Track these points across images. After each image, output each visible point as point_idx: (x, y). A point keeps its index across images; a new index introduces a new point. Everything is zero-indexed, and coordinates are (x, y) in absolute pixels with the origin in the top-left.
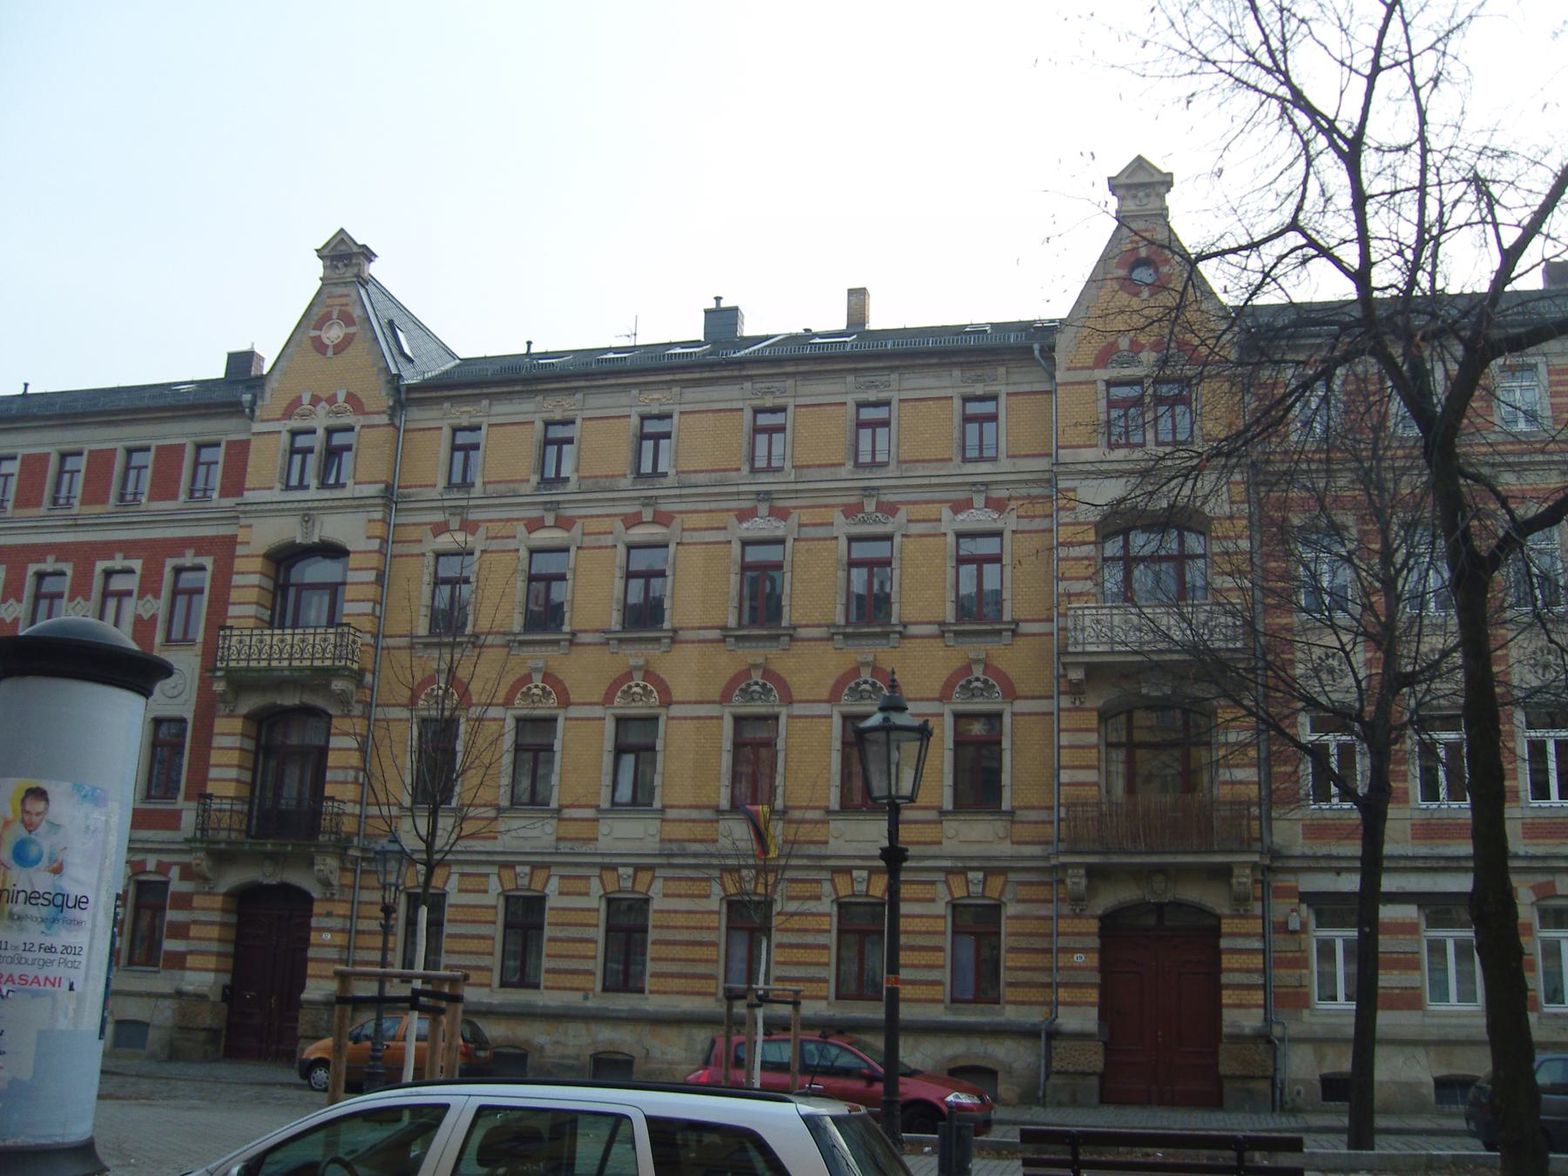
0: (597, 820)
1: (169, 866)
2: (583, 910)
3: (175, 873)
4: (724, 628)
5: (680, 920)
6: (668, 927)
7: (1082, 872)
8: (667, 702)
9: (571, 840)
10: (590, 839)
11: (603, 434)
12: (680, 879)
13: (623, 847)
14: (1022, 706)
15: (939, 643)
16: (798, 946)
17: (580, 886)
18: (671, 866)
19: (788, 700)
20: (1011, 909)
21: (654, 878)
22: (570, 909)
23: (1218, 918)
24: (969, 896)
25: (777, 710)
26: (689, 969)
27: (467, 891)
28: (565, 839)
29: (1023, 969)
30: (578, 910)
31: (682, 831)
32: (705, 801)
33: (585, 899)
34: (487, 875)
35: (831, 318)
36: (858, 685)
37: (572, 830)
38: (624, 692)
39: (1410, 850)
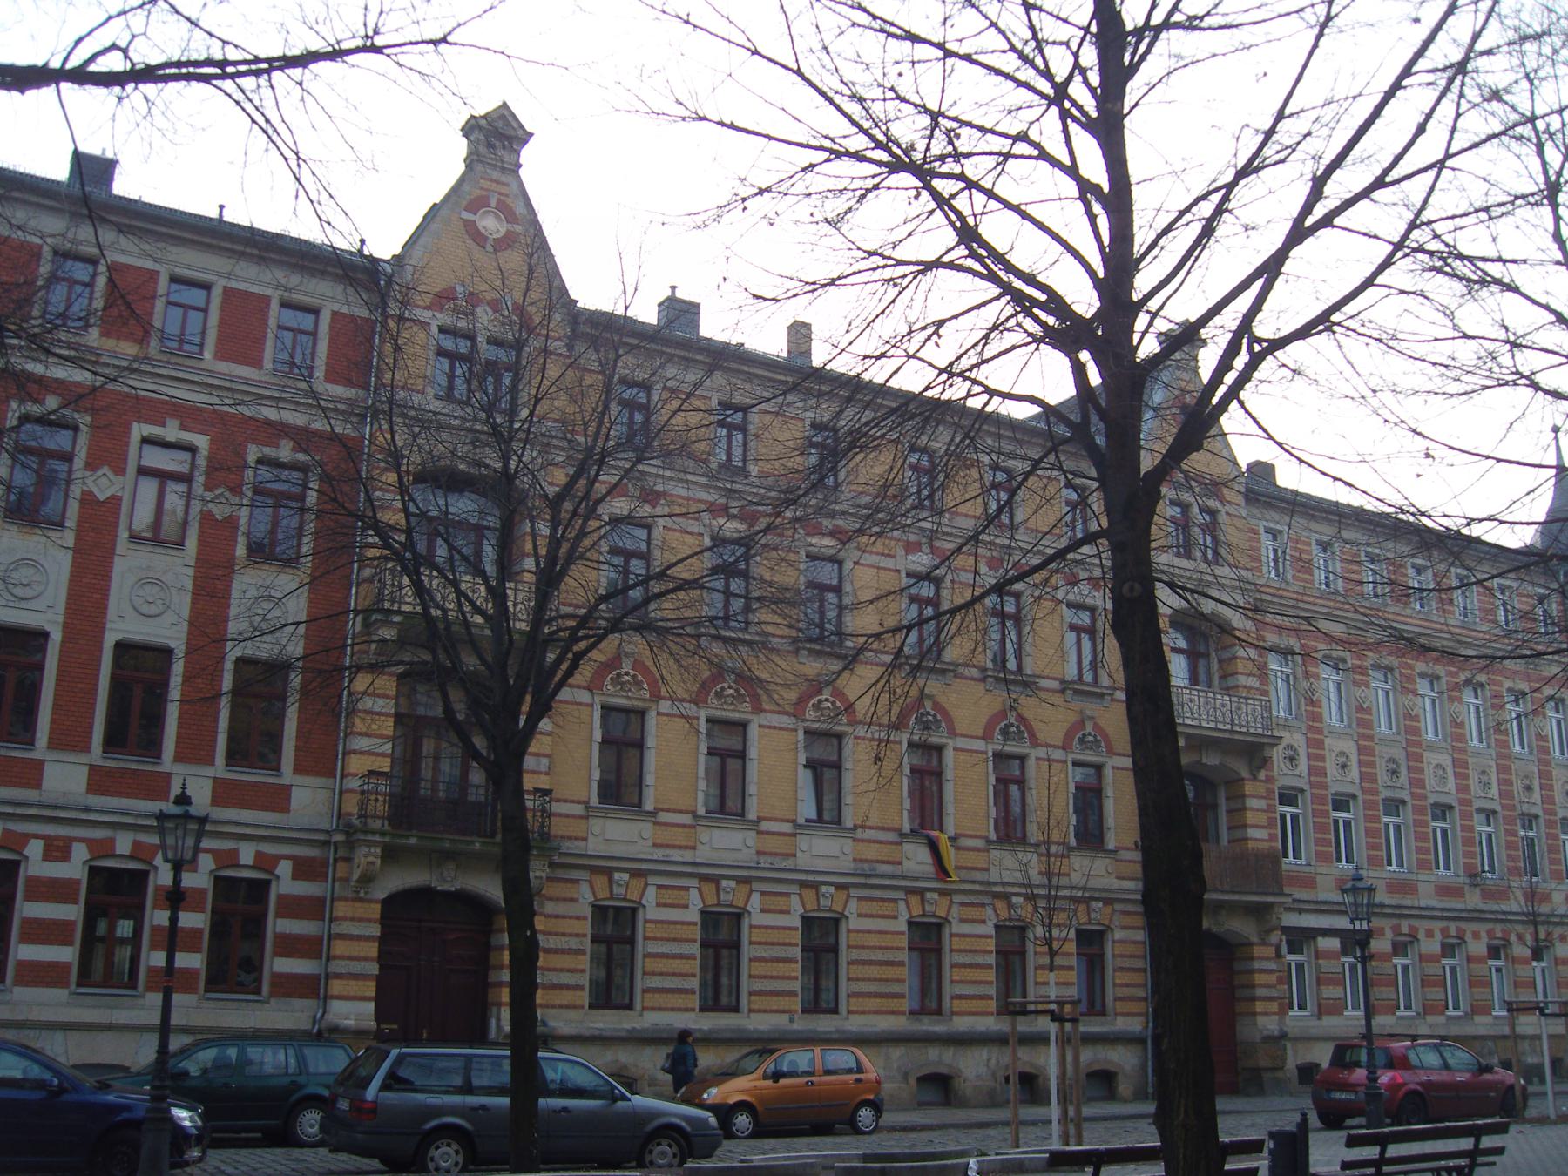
0: (794, 835)
1: (27, 837)
2: (784, 928)
3: (284, 869)
4: (1063, 681)
5: (873, 940)
6: (863, 947)
7: (379, 850)
8: (656, 697)
9: (771, 854)
10: (787, 855)
11: (780, 440)
12: (872, 899)
13: (821, 865)
14: (961, 743)
15: (981, 687)
16: (971, 966)
17: (780, 903)
18: (865, 886)
19: (953, 733)
20: (1118, 935)
21: (849, 896)
22: (773, 928)
23: (1251, 944)
24: (923, 915)
25: (944, 741)
26: (884, 989)
27: (665, 905)
28: (764, 853)
29: (1127, 985)
30: (772, 924)
31: (871, 852)
32: (889, 823)
33: (787, 917)
34: (687, 889)
35: (213, 213)
36: (619, 675)
37: (771, 843)
38: (1081, 741)
39: (1434, 903)
